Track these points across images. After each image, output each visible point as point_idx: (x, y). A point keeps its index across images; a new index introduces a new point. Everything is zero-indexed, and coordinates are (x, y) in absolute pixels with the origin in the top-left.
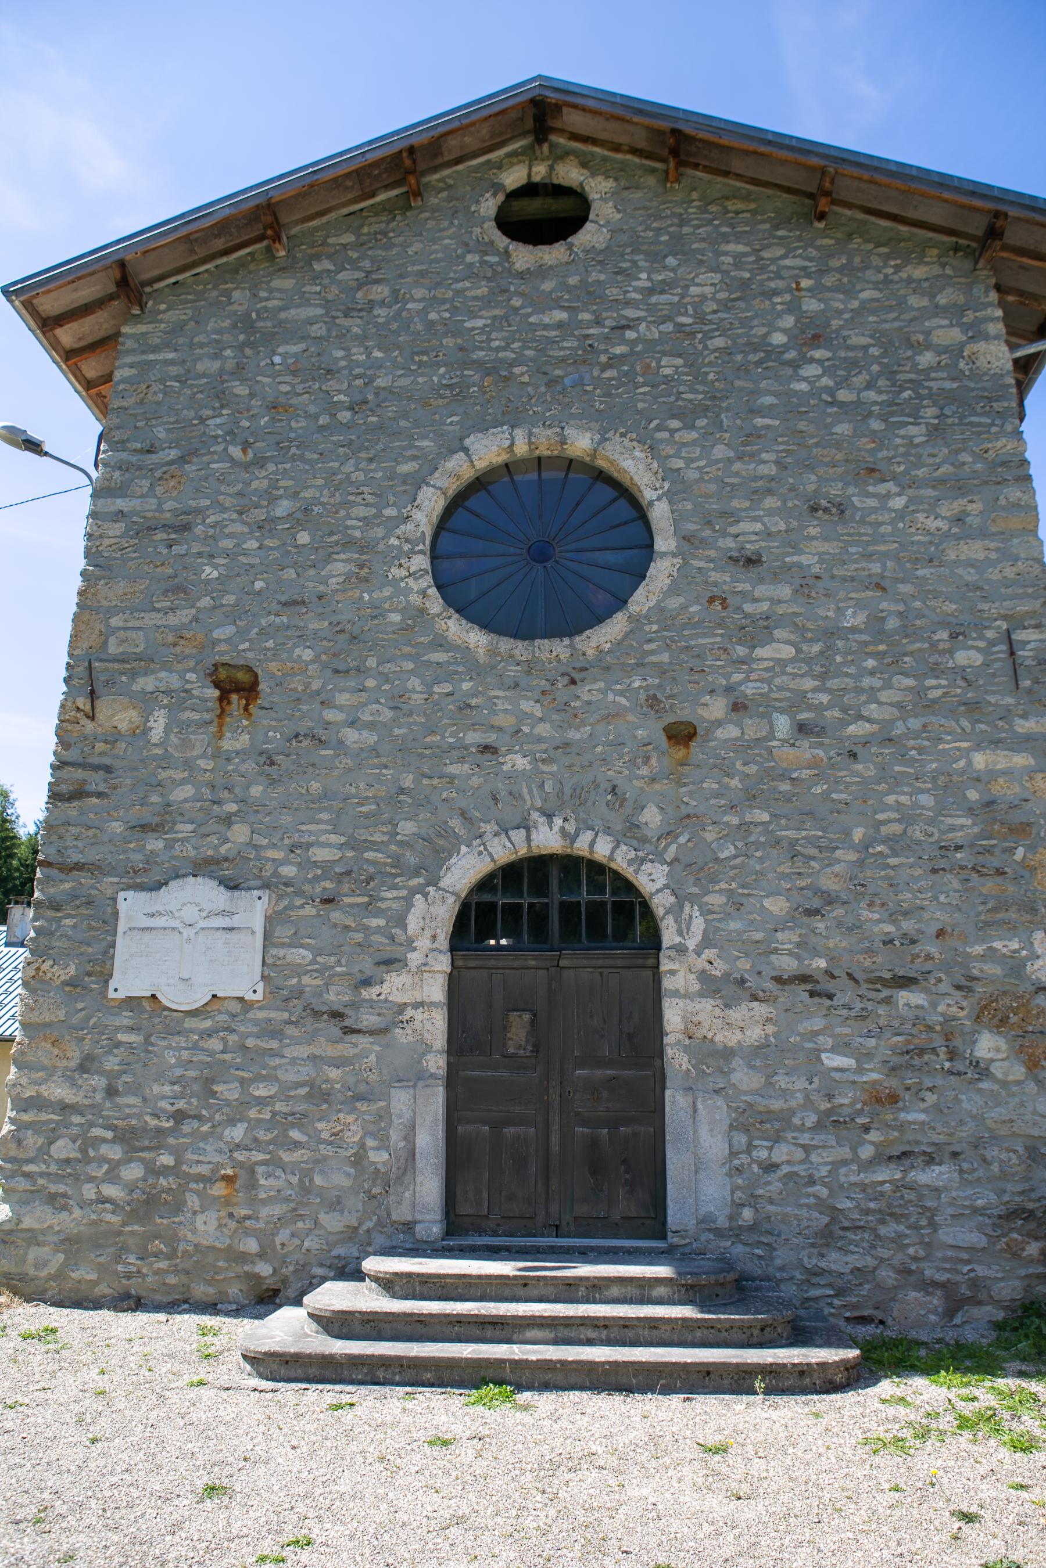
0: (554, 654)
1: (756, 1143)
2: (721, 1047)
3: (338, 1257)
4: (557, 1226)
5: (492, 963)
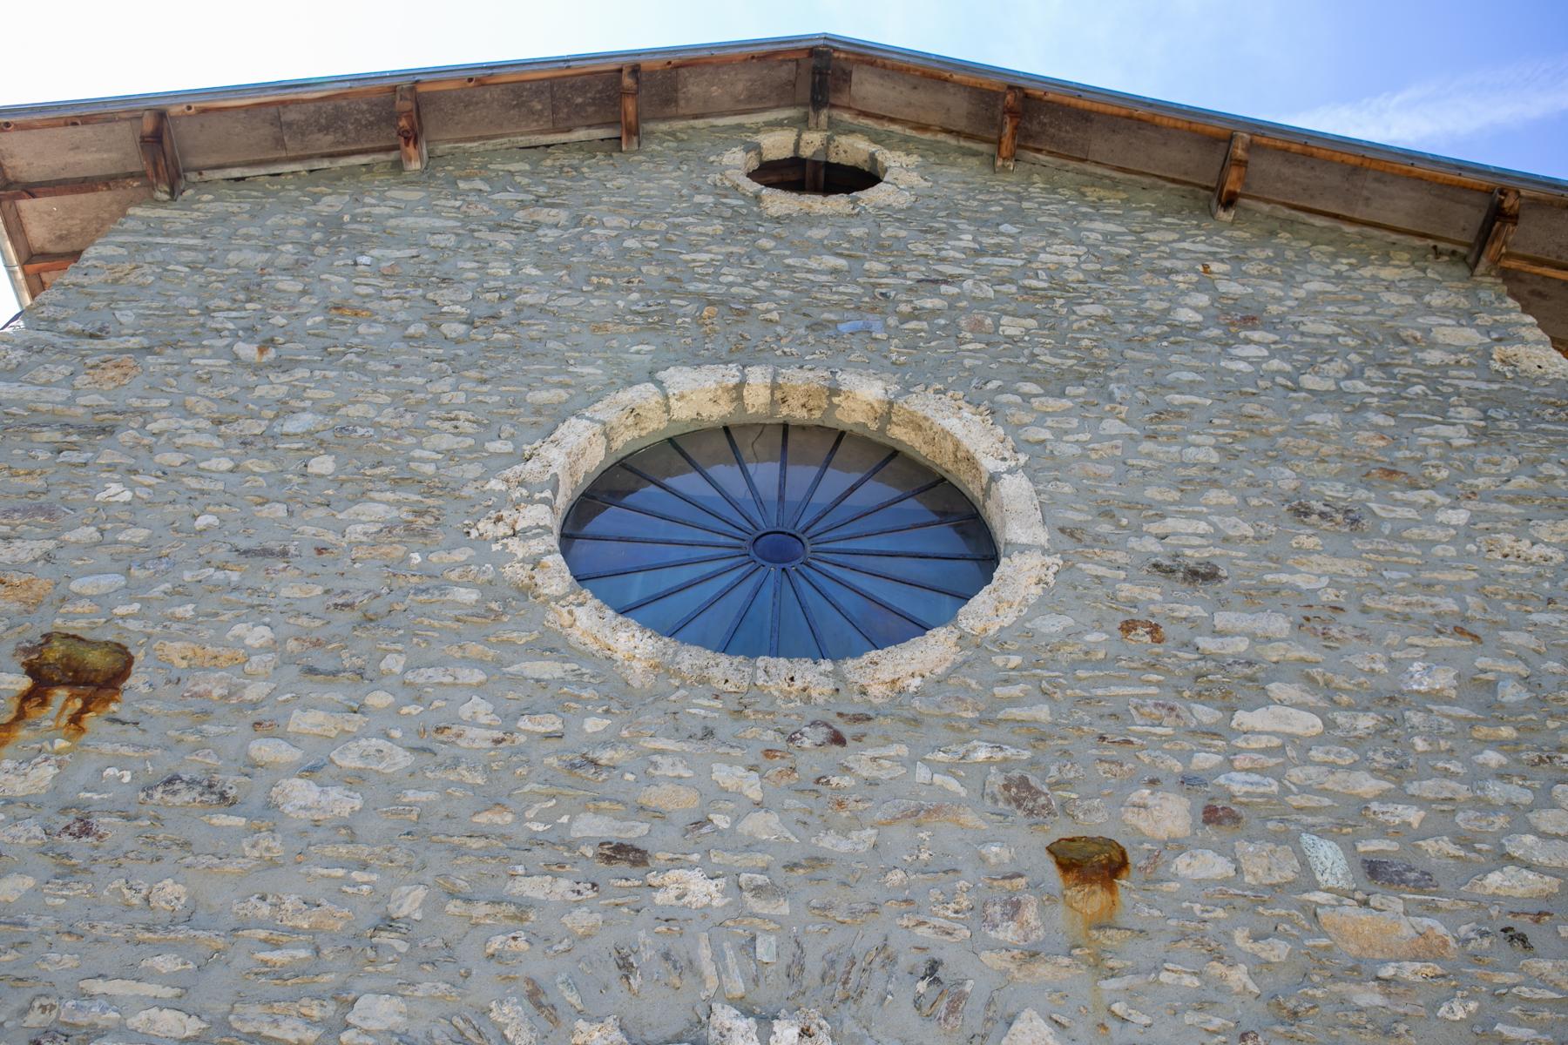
0: (798, 684)
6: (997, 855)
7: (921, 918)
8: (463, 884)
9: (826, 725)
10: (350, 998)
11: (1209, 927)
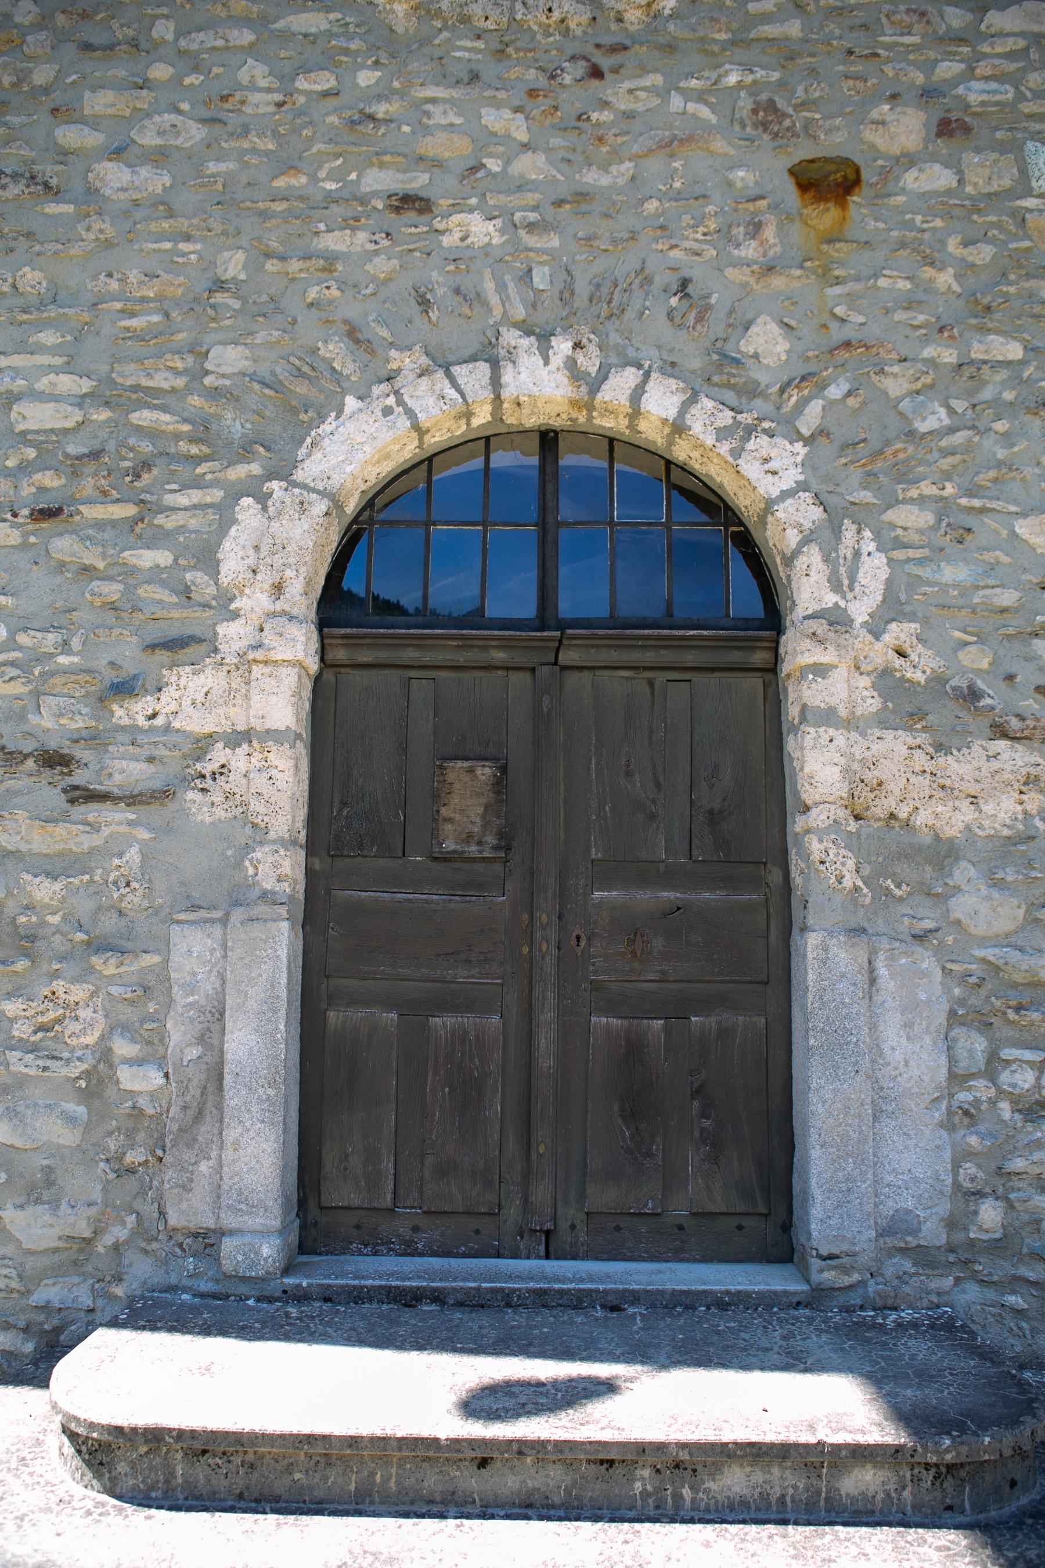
0: (556, 15)
1: (1007, 1053)
2: (926, 839)
3: (45, 1308)
4: (548, 1233)
5: (409, 655)
6: (742, 179)
7: (673, 242)
8: (276, 244)
9: (585, 58)
10: (204, 349)
11: (926, 236)
